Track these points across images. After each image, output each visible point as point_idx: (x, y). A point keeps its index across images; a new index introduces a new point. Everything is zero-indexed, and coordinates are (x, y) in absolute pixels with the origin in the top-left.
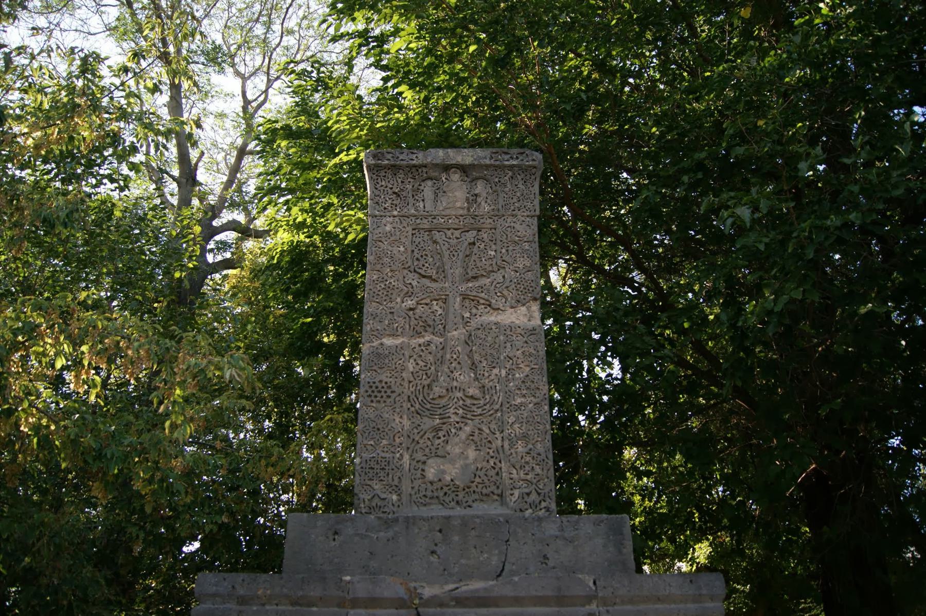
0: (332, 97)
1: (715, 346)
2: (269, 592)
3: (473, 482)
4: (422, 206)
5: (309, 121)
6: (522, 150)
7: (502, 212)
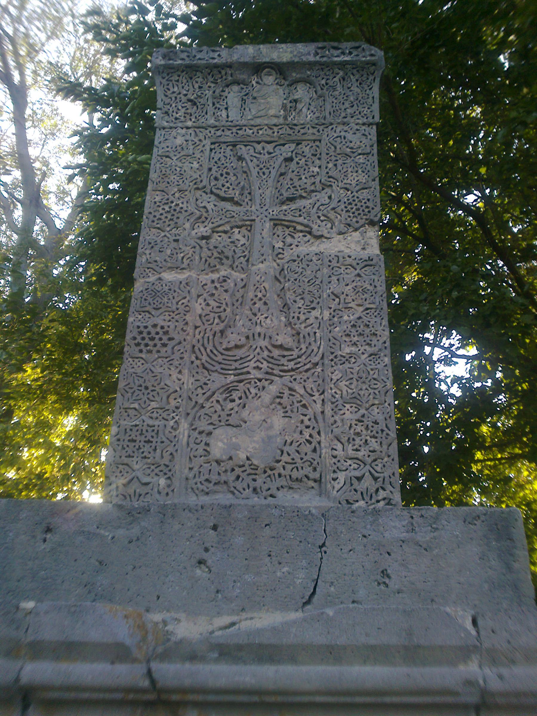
3: (278, 461)
7: (329, 119)
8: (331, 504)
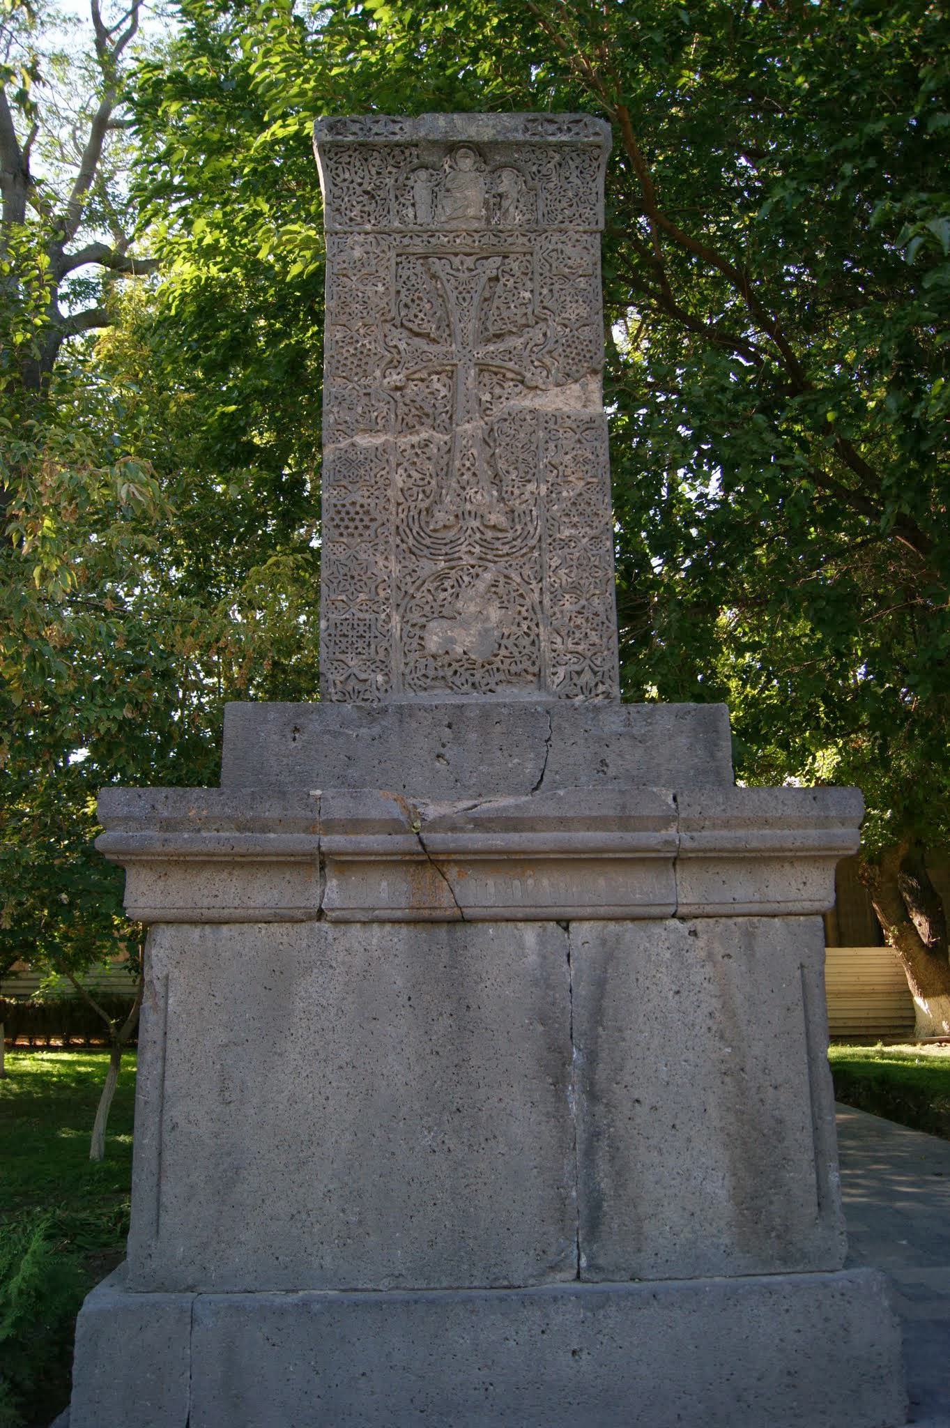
0: (252, 20)
1: (870, 451)
2: (205, 813)
4: (411, 215)
5: (213, 64)
6: (577, 116)
7: (543, 224)
8: (551, 699)
